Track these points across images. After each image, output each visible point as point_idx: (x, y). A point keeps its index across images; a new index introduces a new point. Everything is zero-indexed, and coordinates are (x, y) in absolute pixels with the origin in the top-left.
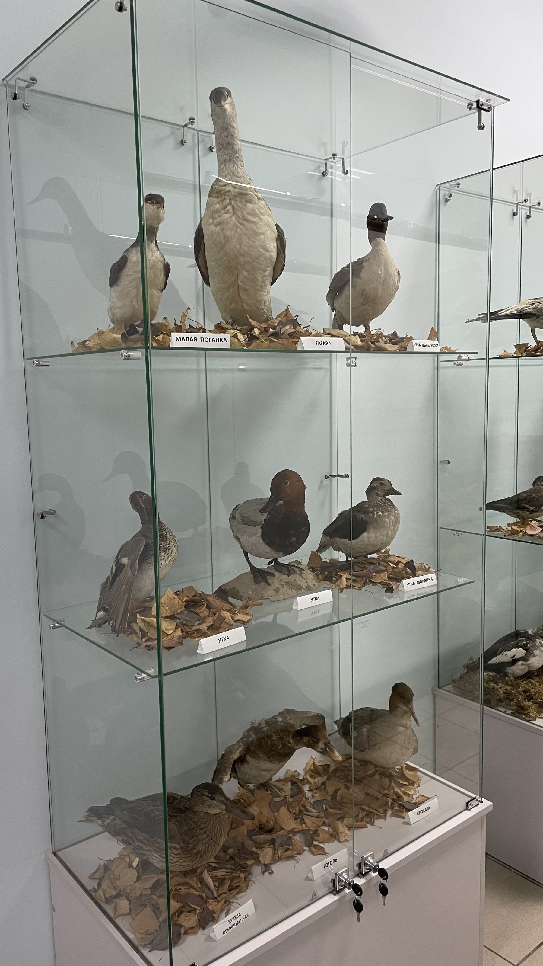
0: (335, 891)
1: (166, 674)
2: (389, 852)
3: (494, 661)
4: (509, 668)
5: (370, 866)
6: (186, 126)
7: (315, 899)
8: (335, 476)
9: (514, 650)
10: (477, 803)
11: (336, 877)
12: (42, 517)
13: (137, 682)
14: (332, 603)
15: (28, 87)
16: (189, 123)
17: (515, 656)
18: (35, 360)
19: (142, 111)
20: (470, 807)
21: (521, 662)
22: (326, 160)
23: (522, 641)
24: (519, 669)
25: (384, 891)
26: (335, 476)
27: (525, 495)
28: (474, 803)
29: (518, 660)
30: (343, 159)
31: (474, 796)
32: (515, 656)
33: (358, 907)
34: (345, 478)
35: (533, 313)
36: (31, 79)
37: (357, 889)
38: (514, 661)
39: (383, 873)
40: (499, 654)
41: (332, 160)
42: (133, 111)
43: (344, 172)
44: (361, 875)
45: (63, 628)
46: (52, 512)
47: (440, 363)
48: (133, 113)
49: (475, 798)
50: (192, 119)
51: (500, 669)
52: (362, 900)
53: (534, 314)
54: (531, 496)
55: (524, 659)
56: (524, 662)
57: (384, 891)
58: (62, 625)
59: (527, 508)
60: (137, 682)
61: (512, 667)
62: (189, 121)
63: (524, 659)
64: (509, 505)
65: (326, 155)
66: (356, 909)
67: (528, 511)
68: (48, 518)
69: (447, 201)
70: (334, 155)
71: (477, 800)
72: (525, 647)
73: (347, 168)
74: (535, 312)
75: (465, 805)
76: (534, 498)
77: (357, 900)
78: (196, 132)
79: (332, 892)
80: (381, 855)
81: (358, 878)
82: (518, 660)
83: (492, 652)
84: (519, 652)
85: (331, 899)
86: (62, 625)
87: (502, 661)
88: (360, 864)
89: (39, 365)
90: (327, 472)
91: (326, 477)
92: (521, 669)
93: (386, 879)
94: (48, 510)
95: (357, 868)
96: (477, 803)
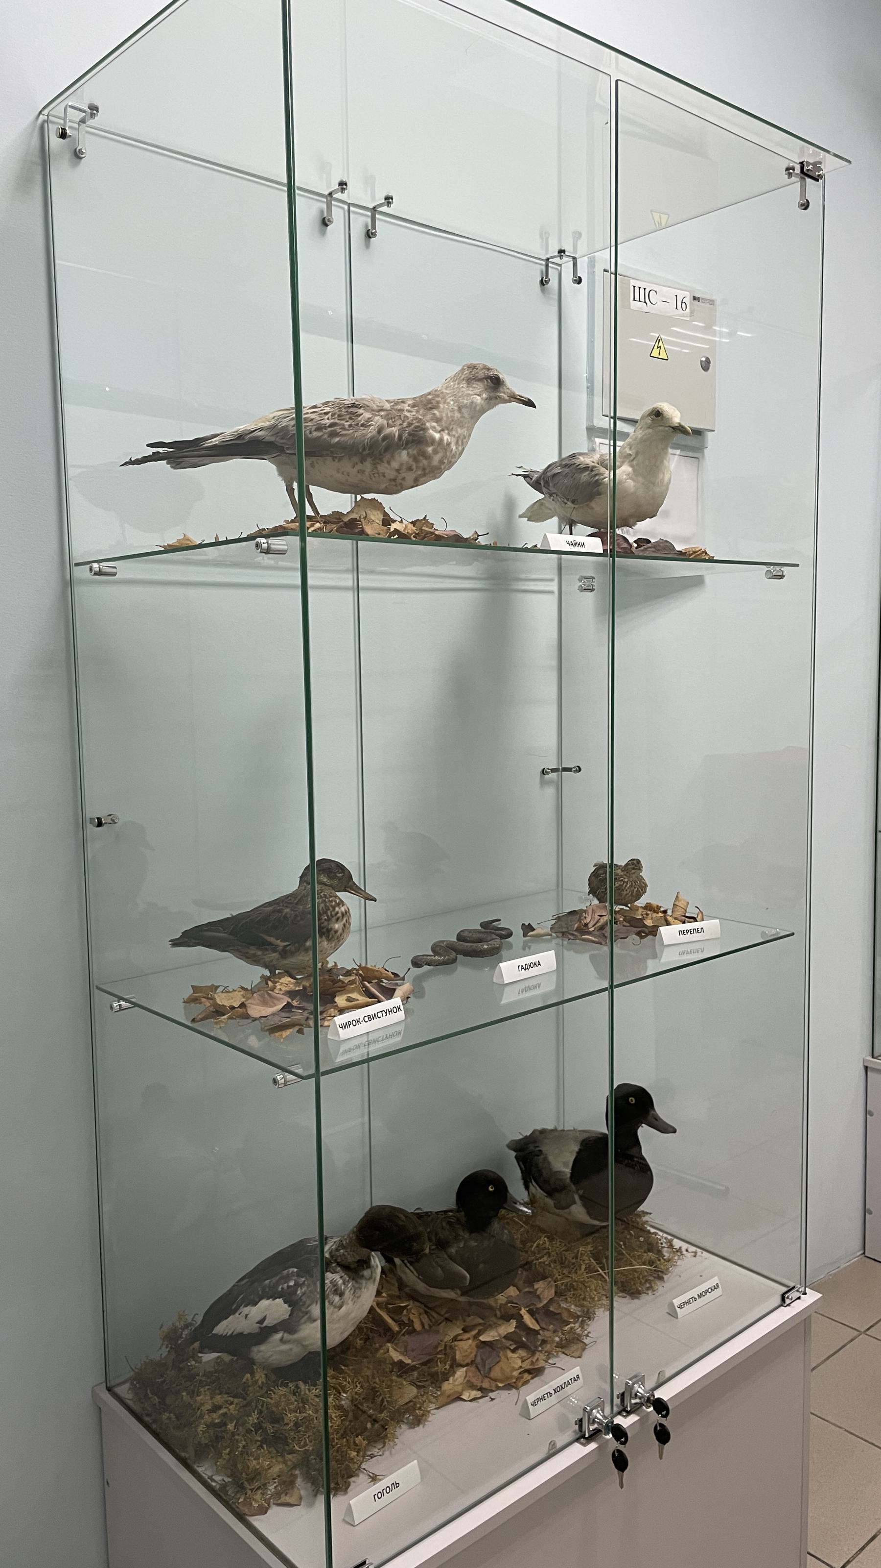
0: (582, 1438)
3: (224, 1328)
4: (255, 1349)
5: (600, 1423)
7: (554, 1451)
9: (264, 1303)
10: (798, 1294)
11: (584, 1415)
12: (100, 824)
14: (555, 974)
15: (83, 121)
17: (264, 1319)
20: (788, 1301)
21: (279, 1336)
23: (288, 1278)
24: (275, 1351)
25: (663, 1435)
27: (271, 908)
28: (794, 1295)
29: (274, 1329)
30: (574, 259)
31: (792, 1284)
32: (264, 1319)
33: (620, 1462)
34: (576, 771)
35: (268, 439)
37: (619, 1433)
38: (264, 1333)
39: (660, 1406)
40: (234, 1313)
44: (625, 1411)
45: (136, 1008)
47: (76, 569)
48: (285, 181)
49: (794, 1288)
51: (240, 1346)
53: (271, 443)
54: (280, 911)
55: (288, 1326)
56: (287, 1336)
57: (663, 1435)
59: (270, 944)
61: (263, 1347)
62: (337, 187)
63: (288, 1326)
64: (231, 934)
66: (616, 1467)
67: (274, 951)
69: (369, 234)
70: (561, 252)
71: (798, 1291)
72: (290, 1298)
73: (582, 273)
74: (273, 439)
76: (285, 917)
77: (661, 1425)
78: (346, 207)
79: (577, 1440)
82: (274, 1329)
83: (225, 1306)
84: (273, 1309)
85: (578, 1451)
87: (238, 1330)
88: (623, 1395)
92: (282, 1352)
93: (624, 1443)
95: (617, 1401)
96: (798, 1294)
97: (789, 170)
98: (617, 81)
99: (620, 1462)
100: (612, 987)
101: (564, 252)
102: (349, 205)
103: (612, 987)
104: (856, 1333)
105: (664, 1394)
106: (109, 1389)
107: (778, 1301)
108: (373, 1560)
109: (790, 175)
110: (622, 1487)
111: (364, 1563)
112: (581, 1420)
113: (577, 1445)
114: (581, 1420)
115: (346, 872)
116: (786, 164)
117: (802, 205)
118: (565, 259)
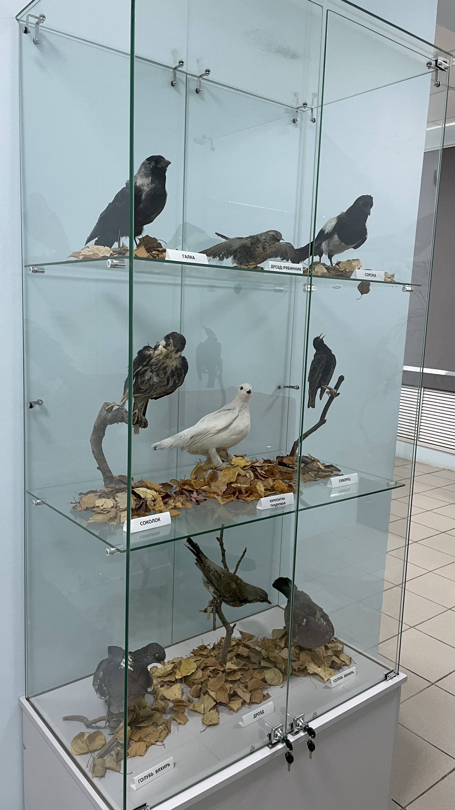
1: (132, 550)
2: (318, 714)
6: (201, 76)
8: (287, 387)
13: (108, 555)
15: (37, 23)
16: (204, 75)
18: (34, 270)
19: (136, 54)
20: (388, 678)
22: (298, 108)
25: (311, 747)
26: (287, 387)
28: (392, 674)
30: (312, 109)
31: (392, 669)
34: (296, 389)
36: (40, 16)
39: (311, 732)
41: (303, 109)
42: (129, 52)
43: (312, 121)
46: (39, 402)
48: (130, 53)
49: (392, 671)
50: (208, 71)
52: (293, 753)
57: (311, 747)
58: (45, 503)
60: (108, 555)
62: (205, 72)
65: (297, 104)
68: (36, 407)
75: (384, 676)
79: (267, 745)
80: (311, 716)
81: (232, 702)
85: (266, 752)
86: (45, 503)
89: (36, 271)
90: (281, 383)
91: (279, 388)
93: (314, 737)
94: (36, 401)
95: (289, 727)
96: (395, 675)
97: (429, 64)
98: (327, 11)
99: (290, 759)
100: (297, 510)
101: (306, 104)
102: (187, 73)
103: (297, 510)
104: (436, 684)
105: (314, 725)
106: (27, 699)
107: (383, 677)
108: (150, 804)
109: (429, 67)
110: (289, 771)
111: (145, 805)
112: (270, 734)
113: (267, 747)
114: (270, 734)
115: (318, 357)
116: (428, 60)
117: (436, 84)
118: (307, 109)
